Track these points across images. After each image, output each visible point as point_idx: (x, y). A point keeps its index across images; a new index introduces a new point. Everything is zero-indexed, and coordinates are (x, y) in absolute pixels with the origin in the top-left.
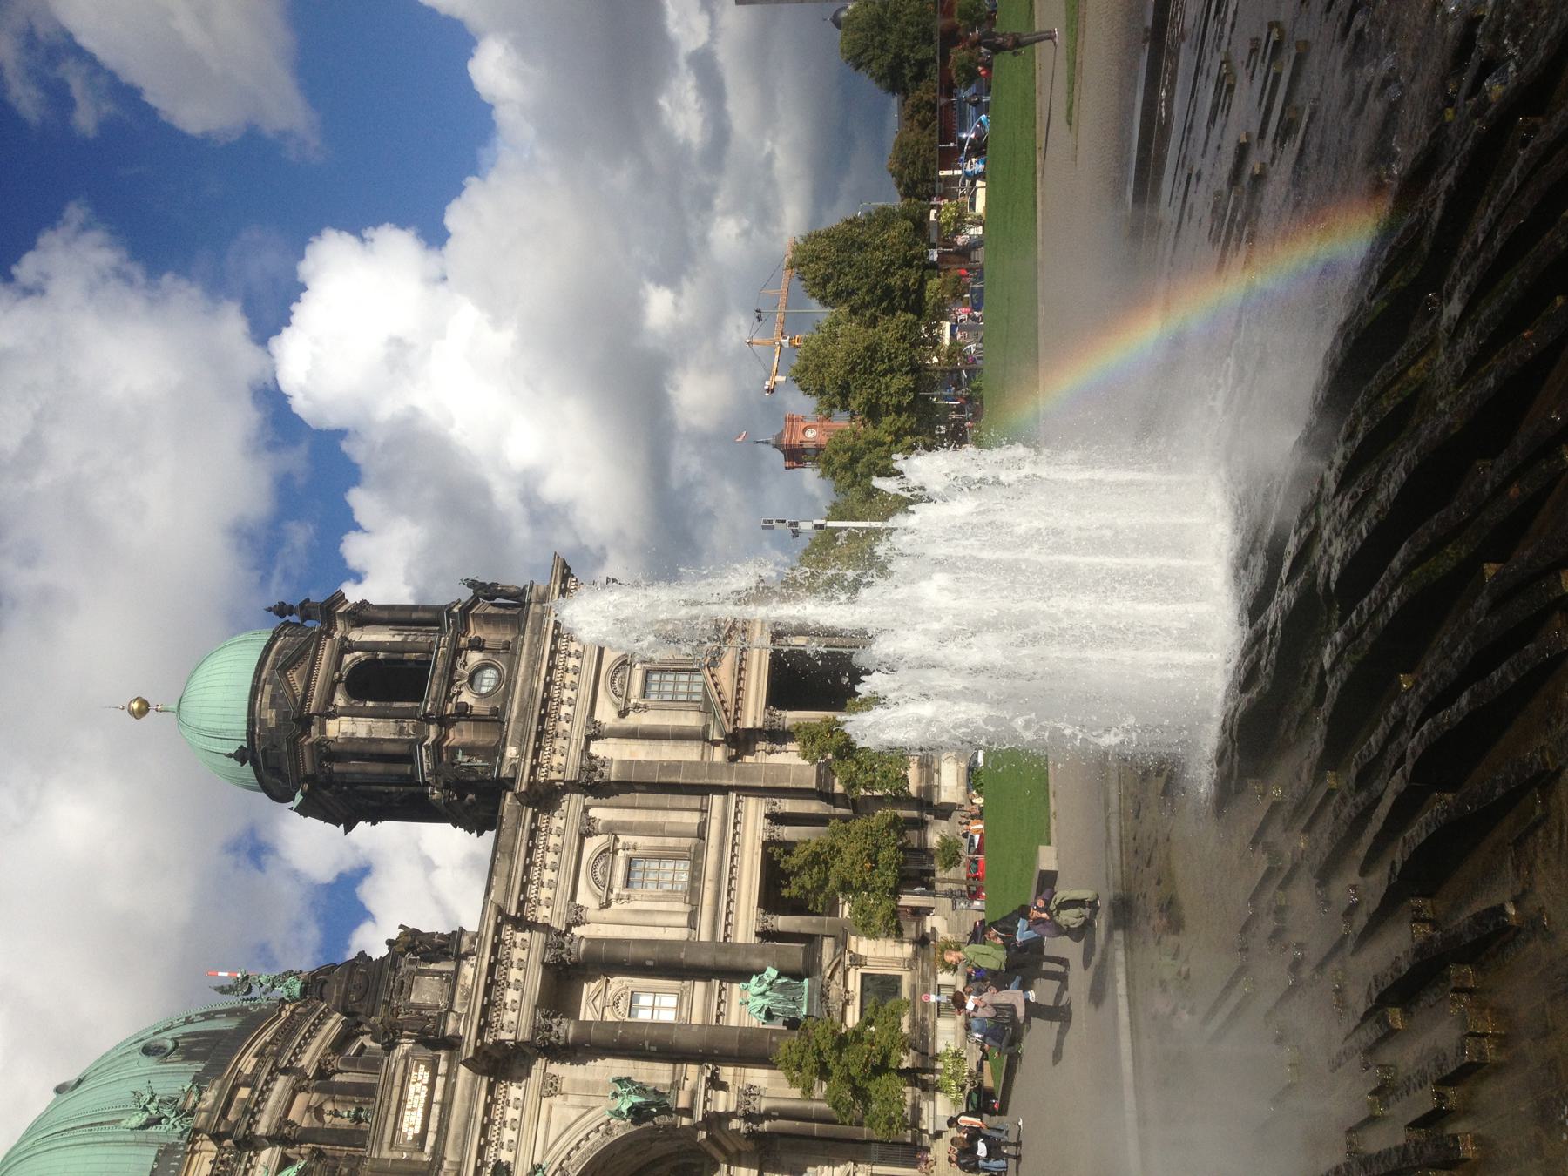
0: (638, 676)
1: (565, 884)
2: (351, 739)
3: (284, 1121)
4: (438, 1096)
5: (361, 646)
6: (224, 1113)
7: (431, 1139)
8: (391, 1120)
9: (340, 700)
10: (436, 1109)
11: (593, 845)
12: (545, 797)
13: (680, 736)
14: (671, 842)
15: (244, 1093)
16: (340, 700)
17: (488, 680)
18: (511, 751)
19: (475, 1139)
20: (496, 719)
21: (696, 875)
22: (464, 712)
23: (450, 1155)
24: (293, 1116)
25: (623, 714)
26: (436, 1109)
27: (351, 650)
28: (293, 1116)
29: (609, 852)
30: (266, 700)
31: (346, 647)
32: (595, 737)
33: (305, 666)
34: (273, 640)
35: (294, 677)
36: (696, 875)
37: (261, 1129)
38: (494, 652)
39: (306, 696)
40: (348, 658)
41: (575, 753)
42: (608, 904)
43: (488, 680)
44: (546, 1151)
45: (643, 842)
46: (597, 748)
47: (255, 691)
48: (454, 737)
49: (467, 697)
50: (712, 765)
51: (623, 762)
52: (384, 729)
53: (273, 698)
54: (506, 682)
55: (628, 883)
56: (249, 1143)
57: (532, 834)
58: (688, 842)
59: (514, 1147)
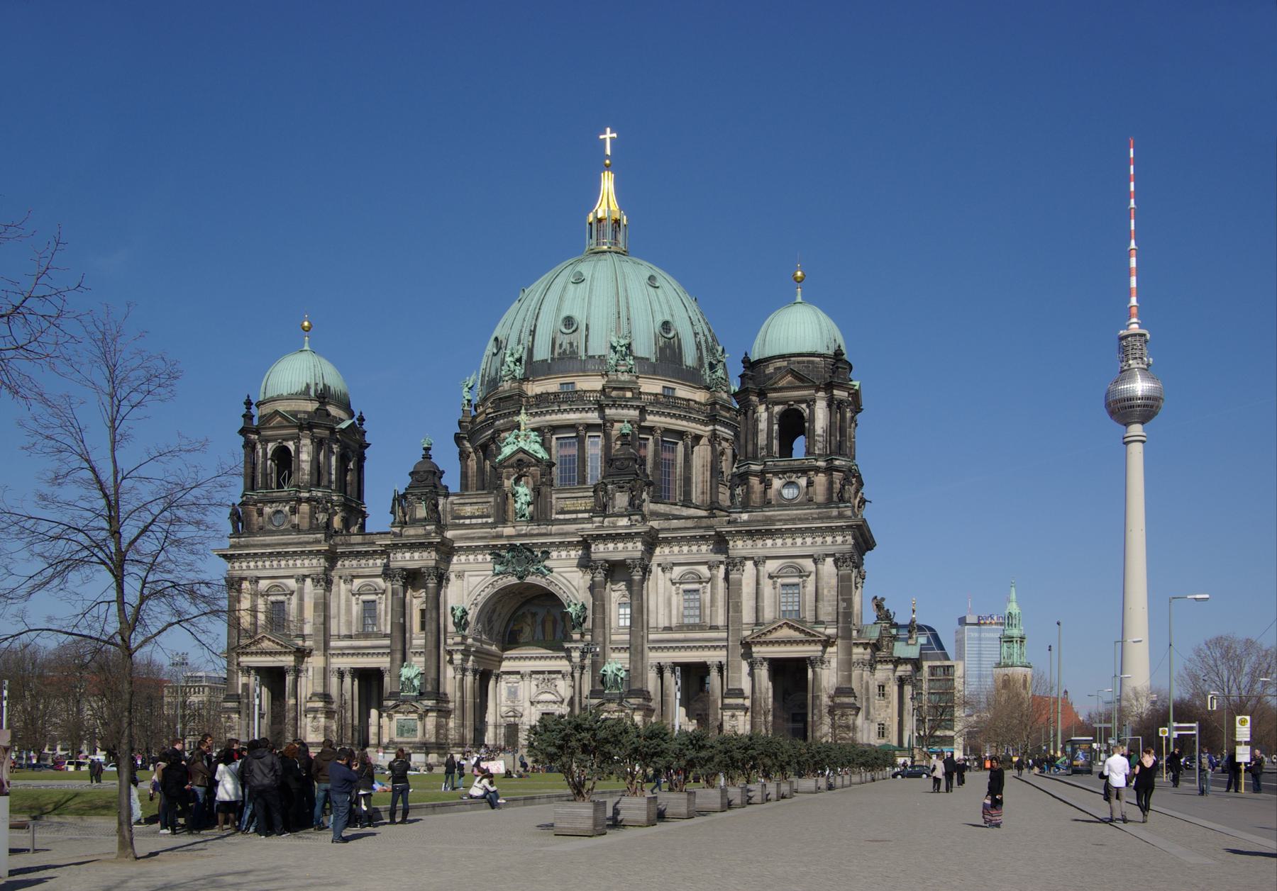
0: (796, 580)
1: (682, 559)
2: (756, 421)
3: (613, 421)
4: (580, 516)
5: (812, 413)
6: (615, 389)
7: (561, 517)
8: (356, 714)
9: (777, 409)
10: (574, 516)
11: (704, 570)
12: (720, 543)
13: (758, 610)
14: (708, 612)
15: (629, 394)
16: (777, 409)
17: (789, 493)
18: (745, 516)
19: (557, 540)
20: (767, 503)
21: (691, 628)
22: (768, 485)
23: (554, 529)
24: (617, 425)
25: (770, 577)
26: (574, 516)
27: (808, 406)
28: (617, 425)
29: (801, 573)
30: (778, 365)
31: (811, 403)
32: (756, 564)
33: (797, 383)
34: (819, 355)
35: (789, 378)
36: (691, 628)
37: (608, 411)
38: (807, 493)
39: (775, 390)
40: (804, 406)
41: (744, 553)
42: (674, 584)
43: (789, 493)
44: (559, 573)
45: (707, 597)
46: (749, 564)
47: (782, 357)
48: (754, 481)
49: (777, 483)
50: (740, 630)
51: (740, 581)
52: (762, 439)
53: (779, 368)
54: (789, 504)
55: (686, 591)
56: (601, 408)
57: (702, 537)
58: (708, 620)
59: (559, 558)
